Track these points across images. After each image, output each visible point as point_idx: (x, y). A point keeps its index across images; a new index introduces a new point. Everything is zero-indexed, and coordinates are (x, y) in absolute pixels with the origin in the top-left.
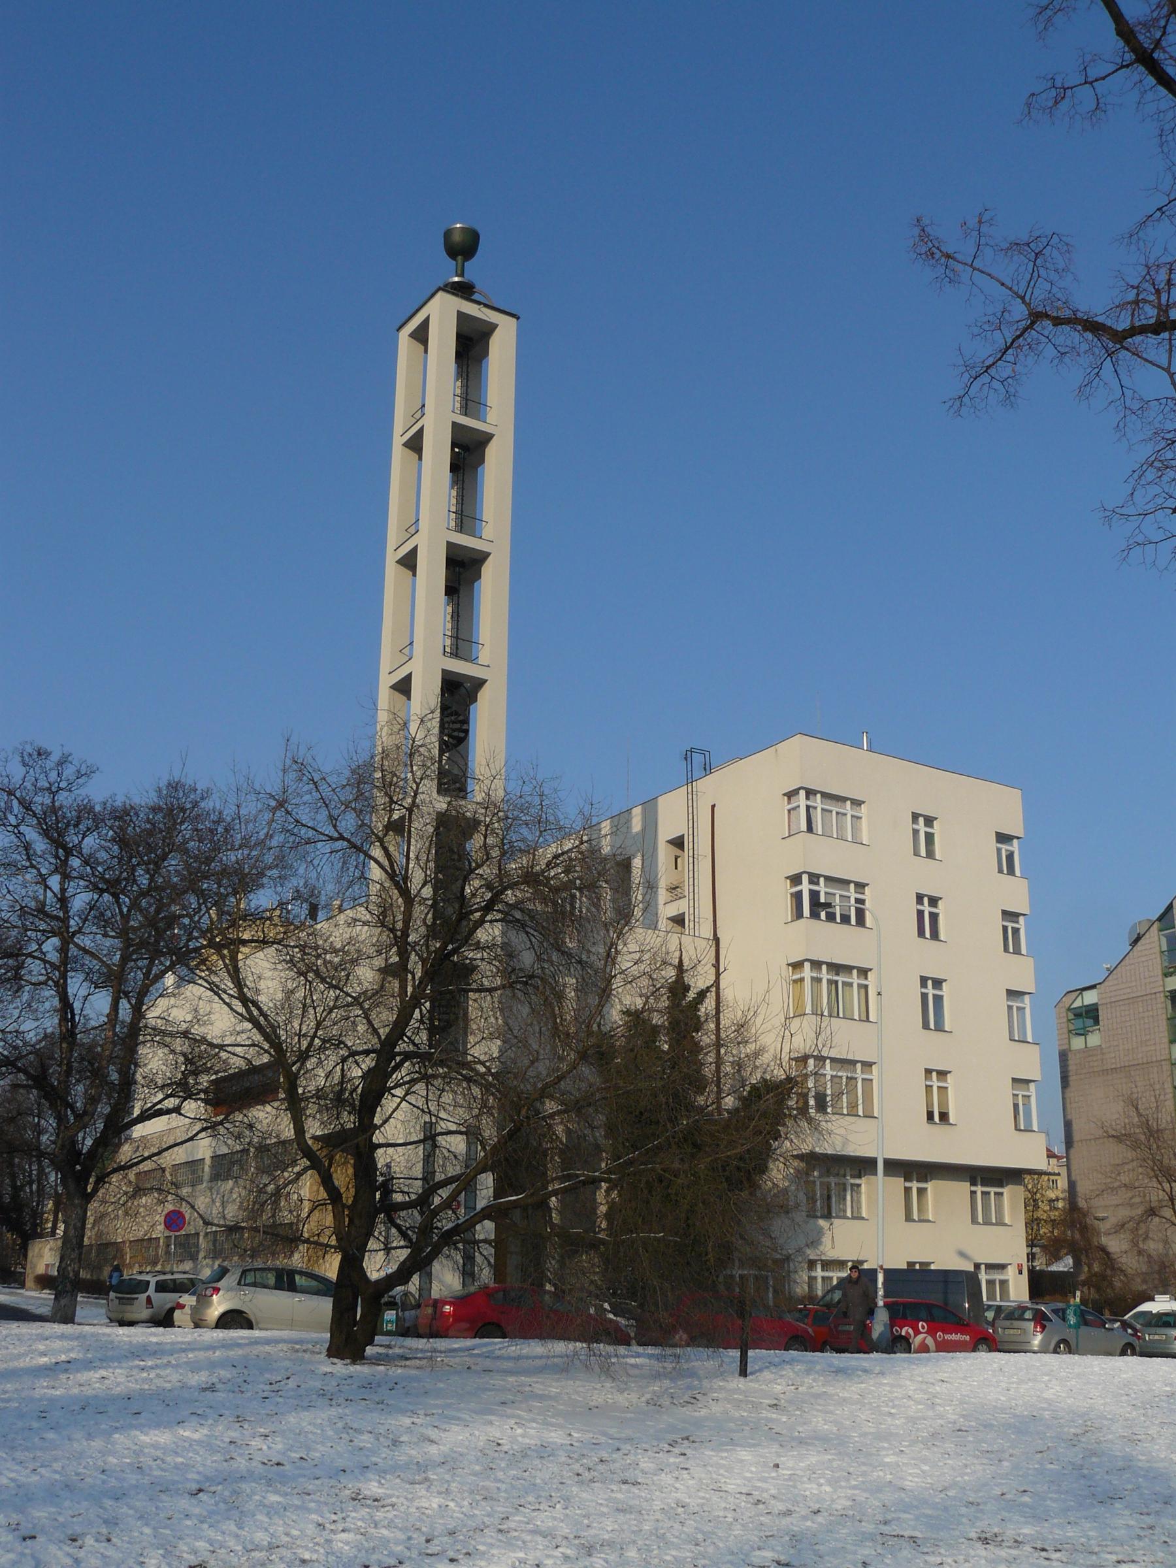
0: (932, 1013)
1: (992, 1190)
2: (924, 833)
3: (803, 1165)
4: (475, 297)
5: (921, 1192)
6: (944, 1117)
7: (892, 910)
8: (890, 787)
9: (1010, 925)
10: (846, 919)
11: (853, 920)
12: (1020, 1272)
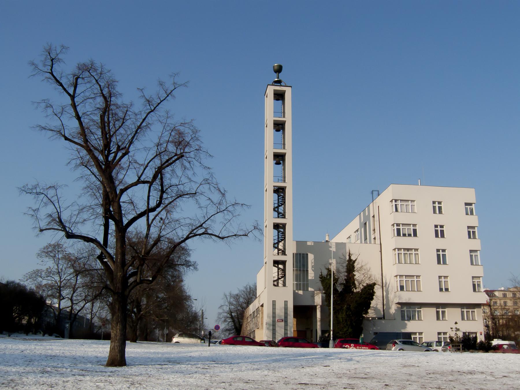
0: (441, 258)
1: (470, 310)
2: (438, 208)
3: (400, 306)
4: (282, 84)
5: (443, 312)
6: (447, 290)
7: (426, 231)
8: (423, 195)
9: (471, 230)
10: (410, 235)
11: (412, 235)
12: (481, 334)
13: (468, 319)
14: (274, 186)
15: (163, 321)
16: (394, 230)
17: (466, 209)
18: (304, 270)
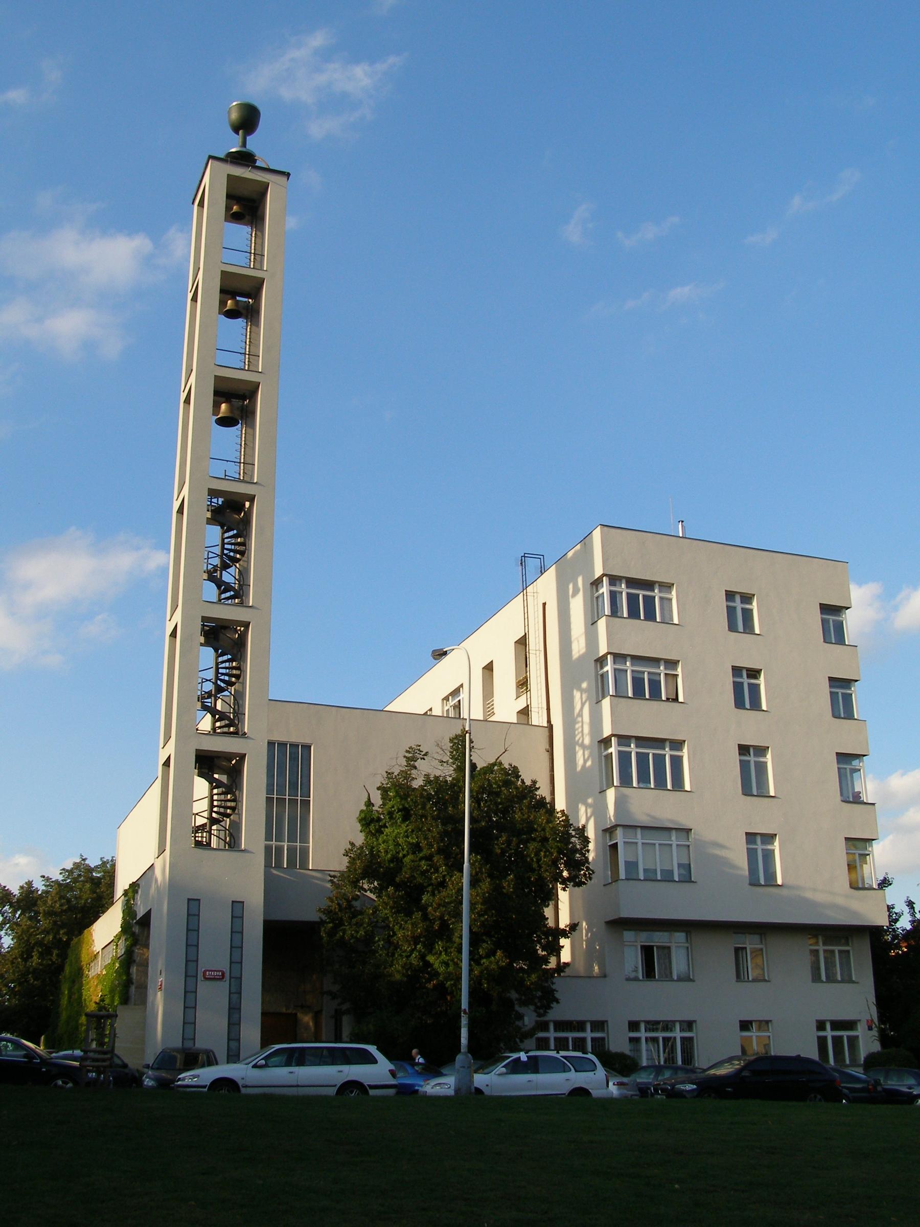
1: (836, 949)
13: (831, 979)
14: (204, 619)
15: (445, 804)
16: (603, 677)
17: (824, 622)
18: (293, 802)
